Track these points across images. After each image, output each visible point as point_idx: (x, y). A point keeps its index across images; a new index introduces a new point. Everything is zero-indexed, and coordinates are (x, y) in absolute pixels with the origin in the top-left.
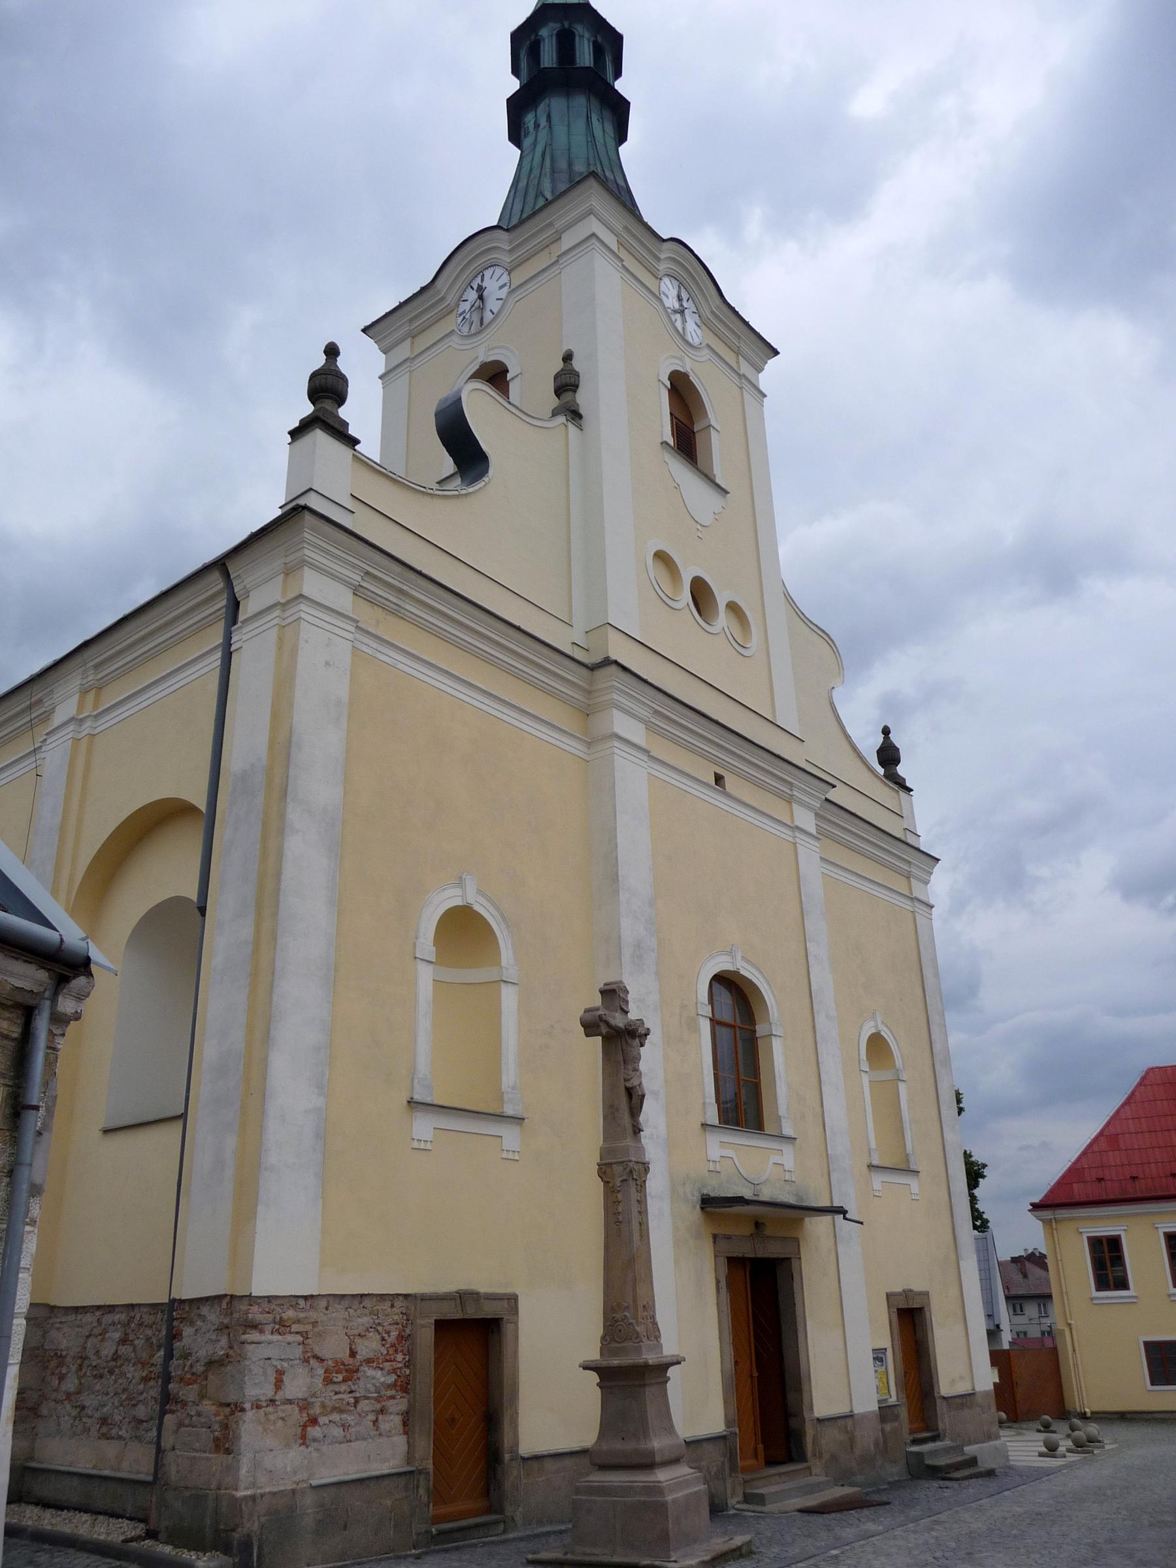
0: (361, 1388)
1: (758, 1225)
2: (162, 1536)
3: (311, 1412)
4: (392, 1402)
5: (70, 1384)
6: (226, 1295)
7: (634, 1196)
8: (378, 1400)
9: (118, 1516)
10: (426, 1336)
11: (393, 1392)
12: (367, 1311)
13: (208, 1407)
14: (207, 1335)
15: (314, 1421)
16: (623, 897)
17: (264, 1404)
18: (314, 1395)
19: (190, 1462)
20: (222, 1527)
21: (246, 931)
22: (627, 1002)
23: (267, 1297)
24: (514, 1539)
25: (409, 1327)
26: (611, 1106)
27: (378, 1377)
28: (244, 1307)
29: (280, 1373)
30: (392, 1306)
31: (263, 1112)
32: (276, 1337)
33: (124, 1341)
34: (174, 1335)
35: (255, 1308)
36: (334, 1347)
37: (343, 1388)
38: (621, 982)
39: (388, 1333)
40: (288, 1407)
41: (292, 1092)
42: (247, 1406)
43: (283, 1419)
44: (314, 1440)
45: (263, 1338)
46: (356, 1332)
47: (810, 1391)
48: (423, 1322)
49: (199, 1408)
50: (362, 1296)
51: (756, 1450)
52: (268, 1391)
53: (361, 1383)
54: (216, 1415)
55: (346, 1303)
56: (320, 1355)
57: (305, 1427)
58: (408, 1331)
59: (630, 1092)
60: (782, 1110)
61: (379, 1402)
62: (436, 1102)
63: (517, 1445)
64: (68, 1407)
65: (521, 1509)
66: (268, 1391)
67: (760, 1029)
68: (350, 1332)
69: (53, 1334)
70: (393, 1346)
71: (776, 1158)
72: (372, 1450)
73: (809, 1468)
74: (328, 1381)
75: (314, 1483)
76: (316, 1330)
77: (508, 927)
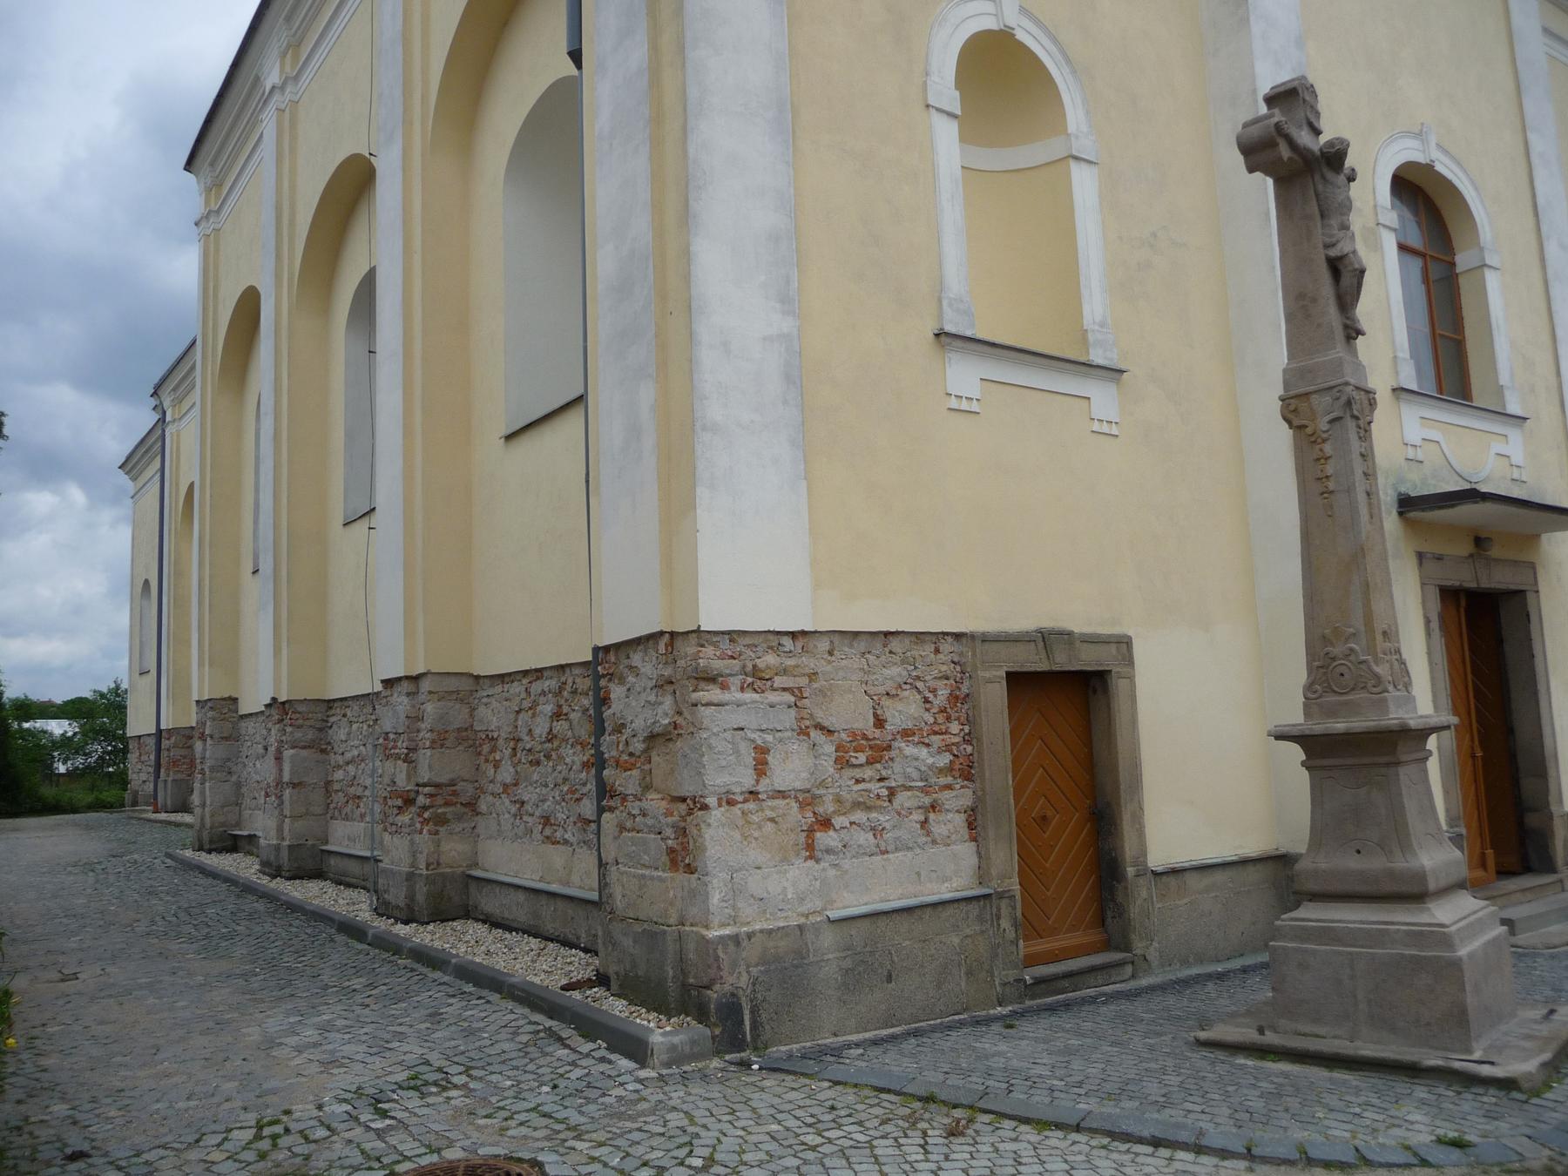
0: (897, 772)
1: (1480, 542)
2: (614, 986)
3: (820, 810)
4: (947, 794)
5: (506, 774)
6: (662, 633)
7: (1356, 446)
8: (924, 791)
9: (572, 946)
10: (994, 696)
11: (949, 780)
12: (897, 659)
13: (655, 803)
14: (644, 695)
15: (826, 823)
16: (1256, 28)
17: (740, 799)
18: (822, 784)
19: (644, 888)
20: (691, 981)
21: (638, 54)
22: (1318, 114)
23: (729, 633)
24: (1152, 989)
25: (967, 683)
26: (1301, 296)
27: (921, 758)
28: (691, 650)
29: (762, 752)
30: (937, 651)
31: (691, 335)
32: (749, 696)
33: (558, 715)
34: (602, 701)
35: (709, 651)
36: (848, 711)
37: (868, 773)
38: (1304, 77)
39: (934, 691)
40: (780, 802)
41: (738, 311)
42: (711, 801)
43: (772, 820)
44: (829, 851)
45: (726, 697)
46: (881, 690)
47: (1558, 777)
48: (987, 675)
49: (644, 804)
50: (887, 634)
51: (1483, 856)
52: (746, 779)
53: (897, 767)
54: (669, 813)
55: (861, 645)
56: (826, 724)
57: (810, 831)
58: (965, 689)
59: (1336, 266)
60: (1504, 378)
61: (927, 793)
62: (979, 336)
63: (1143, 852)
64: (507, 802)
65: (1155, 944)
66: (746, 779)
67: (1463, 261)
68: (872, 690)
69: (482, 711)
70: (943, 710)
71: (1498, 446)
72: (924, 862)
73: (1561, 881)
74: (842, 763)
75: (834, 914)
76: (815, 685)
77: (1074, 72)
